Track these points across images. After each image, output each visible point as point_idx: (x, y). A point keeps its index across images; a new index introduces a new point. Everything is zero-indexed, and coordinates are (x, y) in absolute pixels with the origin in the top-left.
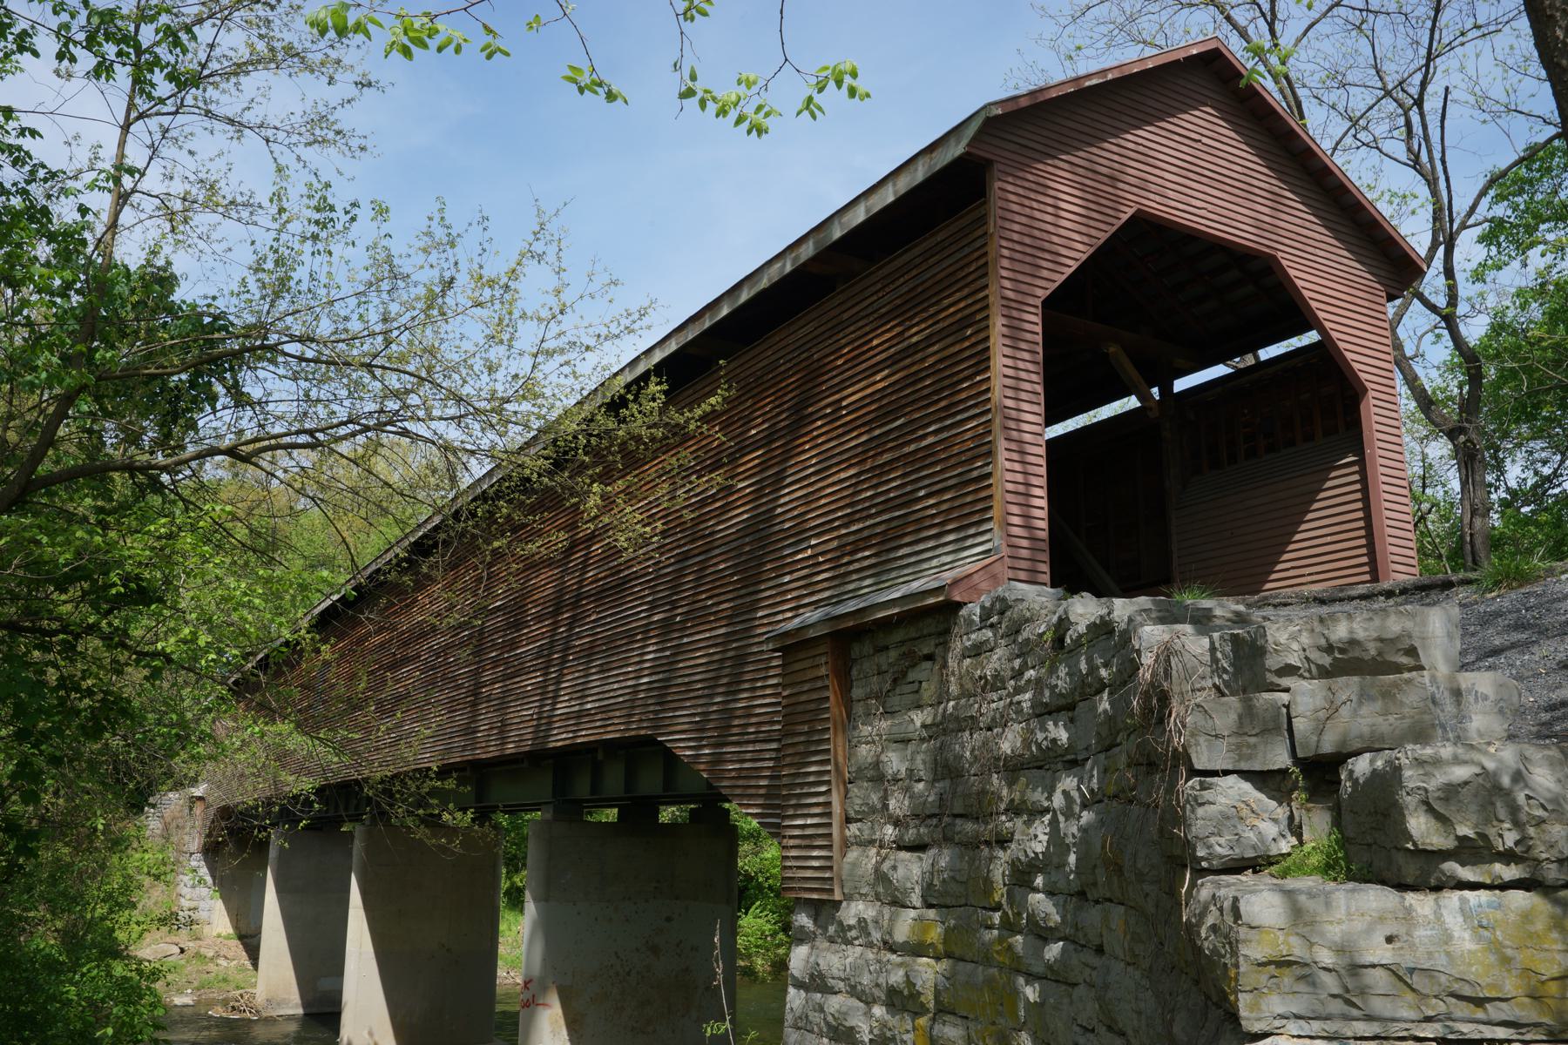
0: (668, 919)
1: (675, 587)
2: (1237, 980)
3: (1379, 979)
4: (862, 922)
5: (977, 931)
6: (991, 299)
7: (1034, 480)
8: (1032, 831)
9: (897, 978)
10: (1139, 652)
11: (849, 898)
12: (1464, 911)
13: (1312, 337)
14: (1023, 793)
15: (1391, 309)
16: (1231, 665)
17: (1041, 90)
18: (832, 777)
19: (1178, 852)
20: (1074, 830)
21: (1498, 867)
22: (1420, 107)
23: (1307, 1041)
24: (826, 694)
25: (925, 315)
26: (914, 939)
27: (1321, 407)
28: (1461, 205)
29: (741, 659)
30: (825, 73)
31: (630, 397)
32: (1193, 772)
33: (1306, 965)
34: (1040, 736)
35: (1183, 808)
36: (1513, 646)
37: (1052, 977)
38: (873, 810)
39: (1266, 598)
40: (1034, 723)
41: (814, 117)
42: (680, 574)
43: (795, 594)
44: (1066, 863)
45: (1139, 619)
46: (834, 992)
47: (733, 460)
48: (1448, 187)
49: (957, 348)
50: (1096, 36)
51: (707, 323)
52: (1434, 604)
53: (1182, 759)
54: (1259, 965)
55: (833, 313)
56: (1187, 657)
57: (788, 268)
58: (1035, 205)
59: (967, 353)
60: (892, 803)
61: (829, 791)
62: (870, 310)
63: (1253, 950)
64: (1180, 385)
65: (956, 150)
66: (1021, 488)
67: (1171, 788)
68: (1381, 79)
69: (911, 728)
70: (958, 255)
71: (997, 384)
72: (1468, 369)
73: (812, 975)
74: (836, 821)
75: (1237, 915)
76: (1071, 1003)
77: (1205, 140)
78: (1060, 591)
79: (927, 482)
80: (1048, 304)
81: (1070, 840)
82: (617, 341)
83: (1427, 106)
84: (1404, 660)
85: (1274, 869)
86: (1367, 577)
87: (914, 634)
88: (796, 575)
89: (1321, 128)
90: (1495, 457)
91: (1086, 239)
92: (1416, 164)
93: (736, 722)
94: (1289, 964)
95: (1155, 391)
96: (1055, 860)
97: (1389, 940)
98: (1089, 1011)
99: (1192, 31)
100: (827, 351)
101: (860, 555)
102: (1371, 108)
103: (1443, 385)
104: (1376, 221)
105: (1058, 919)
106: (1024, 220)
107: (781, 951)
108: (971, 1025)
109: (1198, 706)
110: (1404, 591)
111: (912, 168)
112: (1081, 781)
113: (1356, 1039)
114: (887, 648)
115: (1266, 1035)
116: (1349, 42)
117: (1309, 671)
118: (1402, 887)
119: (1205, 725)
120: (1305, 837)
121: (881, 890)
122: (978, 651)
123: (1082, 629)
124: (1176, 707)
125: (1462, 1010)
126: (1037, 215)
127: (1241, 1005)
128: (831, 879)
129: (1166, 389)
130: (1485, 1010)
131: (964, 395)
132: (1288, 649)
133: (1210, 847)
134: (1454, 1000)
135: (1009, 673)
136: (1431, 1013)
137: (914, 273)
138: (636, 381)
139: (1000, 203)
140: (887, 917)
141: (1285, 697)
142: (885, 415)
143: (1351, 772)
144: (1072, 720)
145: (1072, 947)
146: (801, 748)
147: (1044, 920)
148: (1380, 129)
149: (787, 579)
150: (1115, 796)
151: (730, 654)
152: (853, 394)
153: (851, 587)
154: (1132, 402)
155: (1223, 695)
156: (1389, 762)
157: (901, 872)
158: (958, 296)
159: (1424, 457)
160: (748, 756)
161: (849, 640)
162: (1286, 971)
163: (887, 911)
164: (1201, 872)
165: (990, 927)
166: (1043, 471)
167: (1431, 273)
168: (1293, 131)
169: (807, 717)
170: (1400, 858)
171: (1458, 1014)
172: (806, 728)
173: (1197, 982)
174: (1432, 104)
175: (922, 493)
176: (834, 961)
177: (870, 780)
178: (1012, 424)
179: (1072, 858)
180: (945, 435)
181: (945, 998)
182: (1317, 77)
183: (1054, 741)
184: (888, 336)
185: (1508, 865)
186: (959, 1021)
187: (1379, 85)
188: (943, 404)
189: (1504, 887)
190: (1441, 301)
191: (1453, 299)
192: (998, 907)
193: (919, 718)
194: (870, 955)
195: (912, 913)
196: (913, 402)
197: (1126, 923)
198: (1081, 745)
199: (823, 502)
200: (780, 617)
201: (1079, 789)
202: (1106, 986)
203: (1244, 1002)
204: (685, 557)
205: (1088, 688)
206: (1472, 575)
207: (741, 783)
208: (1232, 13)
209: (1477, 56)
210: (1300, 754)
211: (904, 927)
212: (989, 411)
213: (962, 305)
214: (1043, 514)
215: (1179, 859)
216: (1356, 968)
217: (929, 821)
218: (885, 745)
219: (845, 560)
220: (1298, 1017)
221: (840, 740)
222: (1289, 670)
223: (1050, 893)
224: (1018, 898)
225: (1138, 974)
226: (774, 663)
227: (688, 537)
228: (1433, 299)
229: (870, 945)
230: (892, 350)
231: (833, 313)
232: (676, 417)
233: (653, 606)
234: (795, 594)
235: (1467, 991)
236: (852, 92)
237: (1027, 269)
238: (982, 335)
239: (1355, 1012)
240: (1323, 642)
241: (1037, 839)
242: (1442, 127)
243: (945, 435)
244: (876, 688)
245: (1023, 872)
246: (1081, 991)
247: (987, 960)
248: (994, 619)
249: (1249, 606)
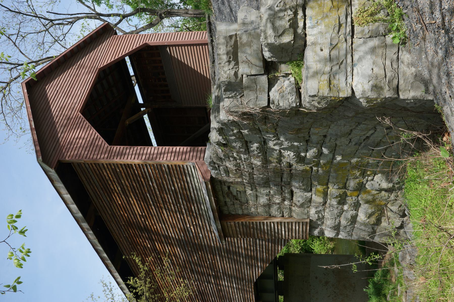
0: (316, 278)
1: (203, 274)
2: (335, 97)
3: (334, 53)
4: (317, 212)
5: (319, 175)
6: (107, 162)
7: (171, 150)
8: (287, 156)
9: (334, 202)
10: (229, 120)
11: (308, 217)
12: (313, 27)
13: (127, 59)
14: (274, 158)
15: (120, 34)
16: (234, 92)
17: (34, 142)
18: (268, 221)
19: (294, 112)
20: (286, 143)
21: (299, 17)
22: (53, 20)
23: (354, 77)
24: (240, 222)
25: (111, 186)
26: (322, 195)
27: (150, 58)
28: (87, 10)
29: (228, 251)
30: (10, 227)
31: (134, 291)
32: (268, 106)
33: (330, 75)
34: (256, 152)
35: (280, 110)
36: (229, 6)
37: (334, 151)
38: (279, 208)
39: (212, 78)
40: (251, 154)
41: (27, 230)
42: (198, 273)
43: (206, 232)
44: (297, 146)
45: (218, 120)
46: (340, 222)
47: (158, 253)
48: (82, 14)
49: (123, 174)
50: (17, 122)
51: (109, 262)
52: (215, 27)
53: (264, 109)
54: (330, 90)
55: (109, 217)
56: (231, 106)
57: (91, 232)
58: (75, 146)
59: (125, 171)
60: (277, 201)
61: (273, 222)
62: (108, 204)
63: (325, 91)
64: (141, 101)
65: (53, 172)
66: (173, 154)
67: (274, 113)
68: (42, 31)
69: (252, 194)
70: (91, 173)
71: (137, 161)
72: (141, 12)
73: (335, 230)
74: (283, 220)
75: (315, 96)
76: (342, 146)
77: (57, 89)
78: (208, 145)
79: (169, 187)
80: (110, 144)
81: (290, 144)
82: (114, 295)
83: (53, 18)
84: (234, 39)
85: (299, 82)
86: (206, 46)
87: (221, 193)
89: (57, 51)
90: (170, 6)
91: (89, 129)
92: (72, 23)
93: (250, 253)
94: (330, 81)
95: (142, 109)
96: (296, 149)
97: (322, 50)
98: (344, 140)
99: (18, 91)
100: (122, 219)
101: (193, 209)
102: (52, 35)
103: (146, 20)
104: (90, 37)
105: (315, 149)
106: (81, 149)
107: (326, 238)
108: (350, 178)
109: (247, 103)
110: (211, 36)
111: (58, 188)
112: (271, 140)
113: (352, 62)
114: (225, 202)
115: (352, 89)
116: (28, 40)
117: (236, 68)
118: (305, 45)
119: (253, 102)
120: (289, 72)
121: (306, 206)
122: (227, 171)
123: (221, 138)
124: (246, 110)
125: (342, 30)
126: (79, 145)
127: (343, 96)
128: (302, 222)
129: (142, 106)
130: (342, 24)
131: (140, 172)
132: (229, 74)
133: (292, 102)
134: (340, 32)
135: (235, 161)
136: (344, 39)
137: (96, 188)
138: (129, 289)
139: (74, 158)
140: (315, 204)
141: (244, 76)
142: (145, 200)
143: (269, 58)
144: (251, 142)
145: (324, 145)
146: (259, 232)
147: (315, 153)
148: (59, 33)
149: (201, 235)
150: (276, 129)
151: (226, 255)
152: (138, 211)
153: (204, 213)
154: (146, 117)
155: (243, 95)
156: (266, 46)
157: (300, 199)
158: (105, 173)
159: (168, 26)
160: (261, 249)
161: (222, 215)
162: (332, 82)
163: (312, 204)
164: (301, 105)
165: (318, 171)
166: (167, 147)
167: (108, 20)
168: (57, 61)
169: (248, 229)
170: (296, 45)
171: (344, 31)
172: (252, 230)
173: (335, 108)
174: (52, 17)
175: (173, 188)
176: (329, 222)
177: (270, 208)
178: (151, 156)
179: (296, 144)
180: (153, 180)
181: (341, 186)
182: (39, 51)
183: (257, 148)
184: (118, 198)
185: (298, 14)
186: (348, 182)
187: (44, 32)
188: (142, 180)
189: (305, 15)
190: (118, 19)
191: (118, 15)
192: (311, 168)
193: (249, 192)
194: (327, 210)
195: (313, 196)
196: (141, 190)
197: (316, 128)
198: (259, 140)
199: (175, 222)
200: (214, 238)
201: (273, 141)
202: (336, 135)
203: (342, 95)
204: (192, 271)
205: (240, 137)
206: (207, 16)
207: (270, 253)
208: (14, 77)
209: (37, 2)
210: (263, 73)
211: (317, 199)
213: (108, 172)
214: (182, 148)
215: (296, 112)
216: (330, 59)
217: (284, 189)
218: (259, 202)
219: (195, 214)
220: (346, 79)
221: (256, 219)
222: (236, 74)
223: (307, 151)
224: (308, 161)
225: (333, 125)
226: (230, 240)
227: (185, 269)
228: (117, 21)
229: (324, 210)
230: (123, 196)
231: (109, 217)
232: (142, 275)
233: (209, 282)
234: (206, 232)
235: (337, 28)
236: (18, 217)
237: (98, 149)
238: (120, 166)
239: (344, 62)
240: (227, 63)
241: (289, 155)
242: (60, 14)
243: (153, 180)
244: (239, 206)
245: (300, 160)
246: (338, 143)
247: (329, 172)
248: (217, 166)
249: (214, 84)
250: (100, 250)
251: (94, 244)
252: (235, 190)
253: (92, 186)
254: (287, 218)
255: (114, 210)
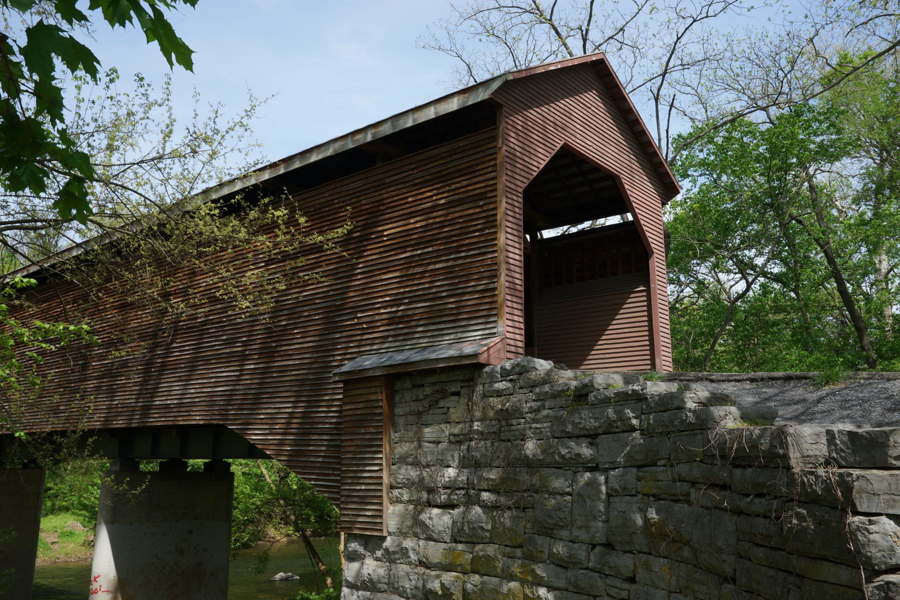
0: (190, 532)
43: (343, 346)
61: (381, 470)
62: (407, 179)
70: (474, 157)
87: (445, 380)
88: (345, 334)
114: (423, 386)
137: (441, 162)
163: (422, 543)
193: (447, 430)
212: (496, 251)
229: (410, 563)
234: (343, 346)
250: (310, 158)
251: (322, 149)
252: (449, 405)
253: (446, 155)
254: (388, 494)
255: (392, 189)
